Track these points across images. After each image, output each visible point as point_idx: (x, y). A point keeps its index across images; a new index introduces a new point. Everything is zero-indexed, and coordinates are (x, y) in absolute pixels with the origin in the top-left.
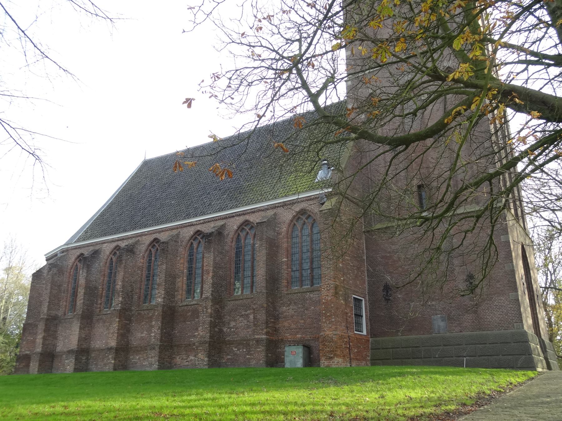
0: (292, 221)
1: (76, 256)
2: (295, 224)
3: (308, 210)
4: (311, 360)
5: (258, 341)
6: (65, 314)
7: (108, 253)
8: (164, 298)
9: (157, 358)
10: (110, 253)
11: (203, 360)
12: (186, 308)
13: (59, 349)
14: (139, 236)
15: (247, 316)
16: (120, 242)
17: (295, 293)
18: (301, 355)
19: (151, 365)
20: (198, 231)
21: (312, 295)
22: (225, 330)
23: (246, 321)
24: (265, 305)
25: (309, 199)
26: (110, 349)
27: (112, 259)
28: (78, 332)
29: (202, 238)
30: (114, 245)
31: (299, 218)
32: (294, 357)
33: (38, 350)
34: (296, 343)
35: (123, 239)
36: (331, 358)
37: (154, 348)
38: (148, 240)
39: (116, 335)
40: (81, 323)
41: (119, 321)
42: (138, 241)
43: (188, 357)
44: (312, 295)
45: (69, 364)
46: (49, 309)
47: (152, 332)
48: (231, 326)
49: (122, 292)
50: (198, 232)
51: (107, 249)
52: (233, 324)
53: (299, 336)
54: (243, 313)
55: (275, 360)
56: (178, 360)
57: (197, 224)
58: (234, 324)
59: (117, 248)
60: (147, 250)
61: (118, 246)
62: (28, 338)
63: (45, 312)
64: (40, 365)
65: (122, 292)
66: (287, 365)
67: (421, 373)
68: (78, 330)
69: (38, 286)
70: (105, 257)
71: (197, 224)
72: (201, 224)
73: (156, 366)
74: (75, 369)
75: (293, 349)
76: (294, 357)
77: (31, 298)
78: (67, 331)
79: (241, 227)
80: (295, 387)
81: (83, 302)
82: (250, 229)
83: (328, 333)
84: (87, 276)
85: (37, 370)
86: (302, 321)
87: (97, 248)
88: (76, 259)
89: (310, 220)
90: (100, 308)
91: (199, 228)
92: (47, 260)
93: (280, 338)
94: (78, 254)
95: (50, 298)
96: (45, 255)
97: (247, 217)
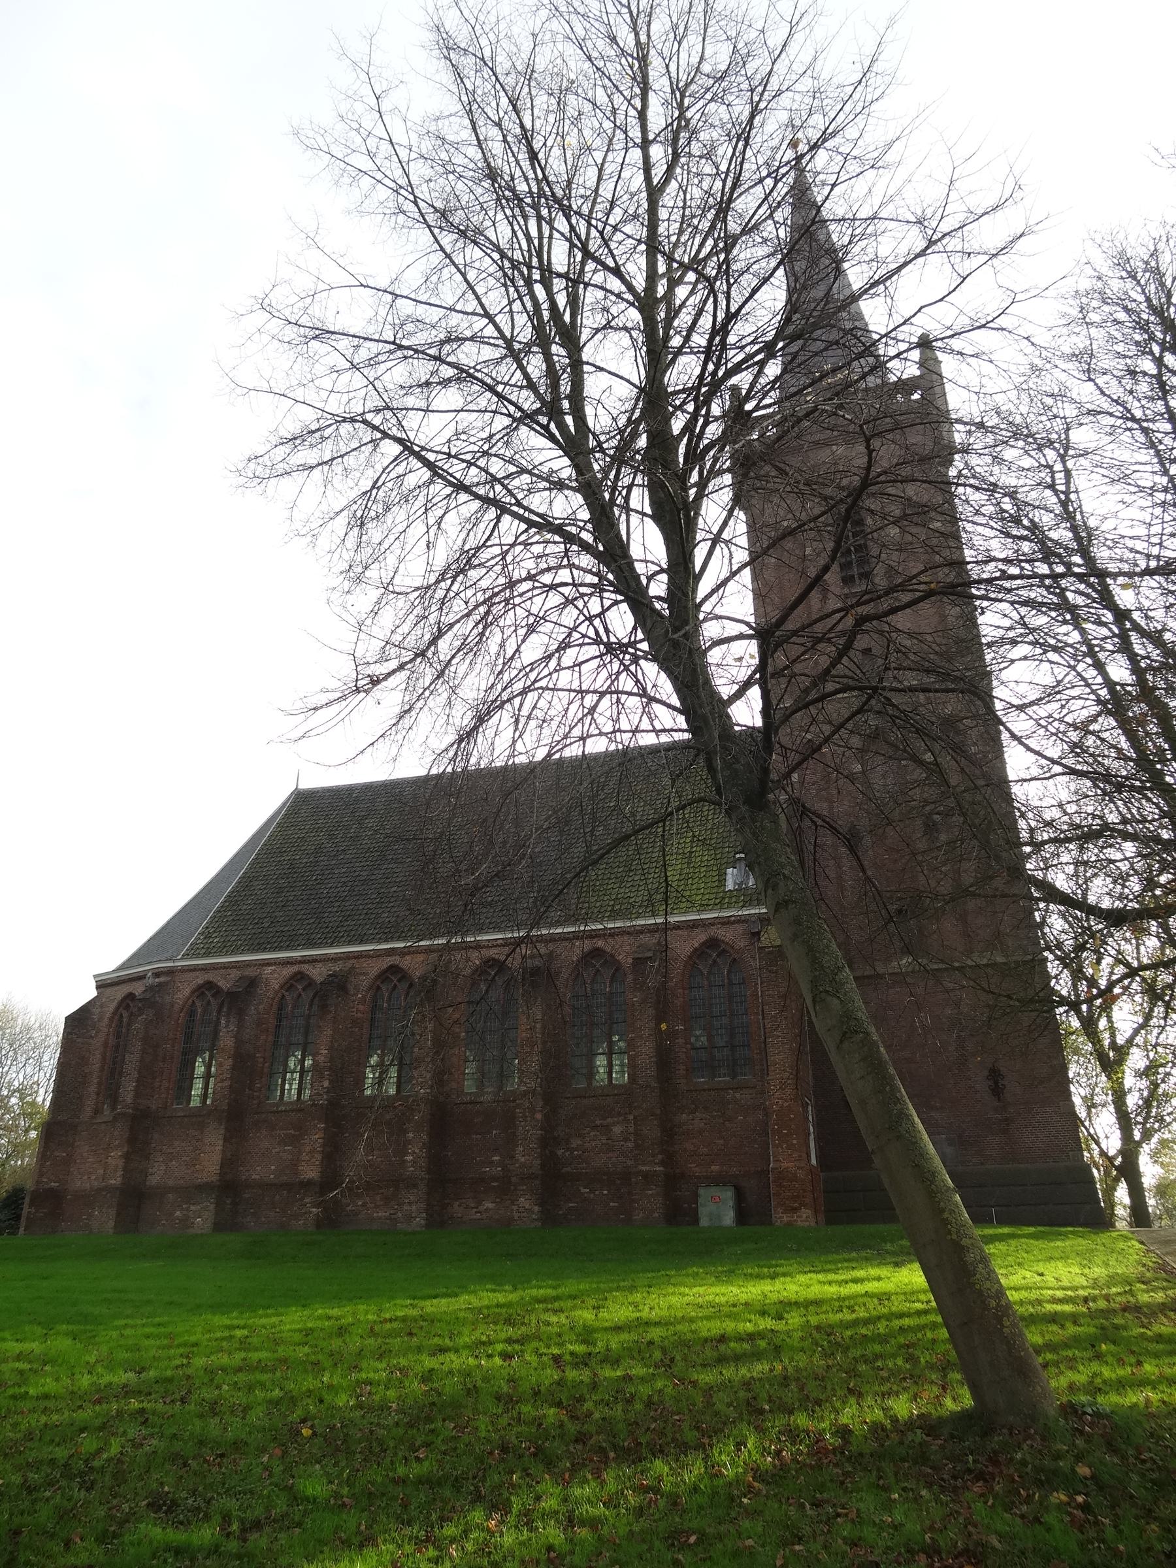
0: (690, 957)
1: (193, 985)
2: (283, 996)
3: (723, 941)
4: (749, 1213)
5: (646, 1176)
6: (166, 1108)
7: (277, 987)
8: (431, 1087)
9: (422, 1206)
10: (281, 987)
11: (530, 1211)
12: (470, 1106)
13: (153, 1180)
14: (355, 958)
15: (608, 1128)
16: (306, 966)
17: (704, 1090)
18: (731, 1203)
19: (409, 1218)
20: (598, 949)
21: (738, 1095)
22: (560, 1152)
23: (604, 1138)
24: (658, 1112)
25: (725, 922)
26: (204, 1188)
27: (283, 996)
28: (220, 1148)
29: (213, 996)
30: (290, 970)
31: (292, 986)
32: (718, 1208)
33: (113, 1182)
34: (718, 1181)
35: (340, 959)
36: (795, 1210)
37: (415, 1186)
38: (375, 968)
39: (319, 1156)
40: (226, 1129)
41: (325, 1129)
42: (353, 968)
43: (480, 1203)
44: (738, 1095)
45: (104, 1218)
46: (138, 1094)
47: (407, 1154)
48: (574, 1145)
49: (330, 1069)
50: (209, 985)
51: (275, 978)
52: (575, 1143)
53: (715, 1168)
54: (598, 1122)
55: (681, 1212)
56: (457, 1209)
57: (488, 946)
58: (579, 1142)
59: (299, 976)
60: (371, 988)
61: (299, 973)
62: (57, 1154)
63: (129, 1100)
64: (118, 1214)
65: (330, 1069)
66: (704, 1222)
67: (1013, 1236)
68: (221, 1142)
69: (79, 1040)
70: (270, 994)
71: (488, 946)
72: (497, 946)
73: (420, 1221)
74: (215, 1224)
75: (714, 1191)
76: (718, 1208)
77: (63, 1067)
78: (176, 1143)
79: (699, 954)
80: (878, 1265)
81: (231, 1086)
82: (399, 981)
83: (785, 1165)
84: (238, 1032)
85: (111, 1223)
86: (722, 1142)
87: (250, 972)
88: (193, 992)
89: (405, 985)
90: (258, 1097)
91: (713, 931)
92: (98, 987)
93: (677, 1171)
94: (200, 981)
95: (139, 1073)
96: (95, 976)
97: (305, 968)
